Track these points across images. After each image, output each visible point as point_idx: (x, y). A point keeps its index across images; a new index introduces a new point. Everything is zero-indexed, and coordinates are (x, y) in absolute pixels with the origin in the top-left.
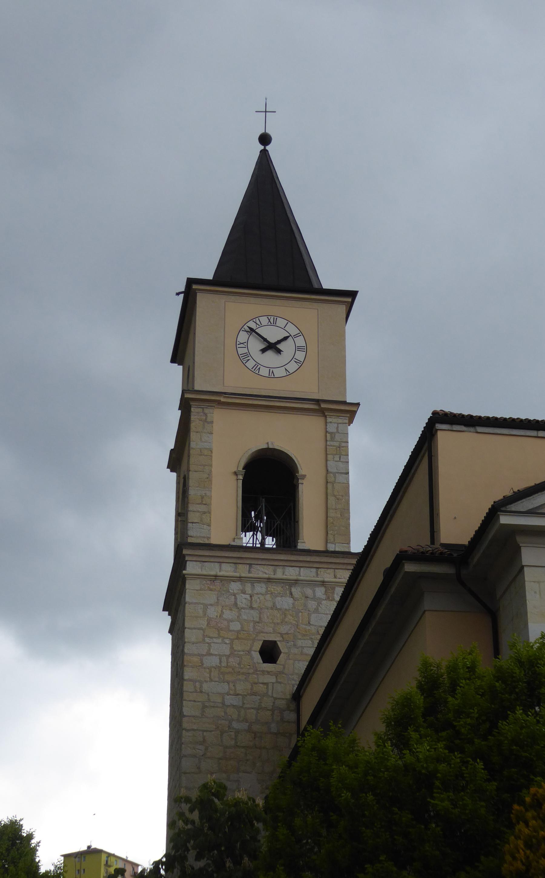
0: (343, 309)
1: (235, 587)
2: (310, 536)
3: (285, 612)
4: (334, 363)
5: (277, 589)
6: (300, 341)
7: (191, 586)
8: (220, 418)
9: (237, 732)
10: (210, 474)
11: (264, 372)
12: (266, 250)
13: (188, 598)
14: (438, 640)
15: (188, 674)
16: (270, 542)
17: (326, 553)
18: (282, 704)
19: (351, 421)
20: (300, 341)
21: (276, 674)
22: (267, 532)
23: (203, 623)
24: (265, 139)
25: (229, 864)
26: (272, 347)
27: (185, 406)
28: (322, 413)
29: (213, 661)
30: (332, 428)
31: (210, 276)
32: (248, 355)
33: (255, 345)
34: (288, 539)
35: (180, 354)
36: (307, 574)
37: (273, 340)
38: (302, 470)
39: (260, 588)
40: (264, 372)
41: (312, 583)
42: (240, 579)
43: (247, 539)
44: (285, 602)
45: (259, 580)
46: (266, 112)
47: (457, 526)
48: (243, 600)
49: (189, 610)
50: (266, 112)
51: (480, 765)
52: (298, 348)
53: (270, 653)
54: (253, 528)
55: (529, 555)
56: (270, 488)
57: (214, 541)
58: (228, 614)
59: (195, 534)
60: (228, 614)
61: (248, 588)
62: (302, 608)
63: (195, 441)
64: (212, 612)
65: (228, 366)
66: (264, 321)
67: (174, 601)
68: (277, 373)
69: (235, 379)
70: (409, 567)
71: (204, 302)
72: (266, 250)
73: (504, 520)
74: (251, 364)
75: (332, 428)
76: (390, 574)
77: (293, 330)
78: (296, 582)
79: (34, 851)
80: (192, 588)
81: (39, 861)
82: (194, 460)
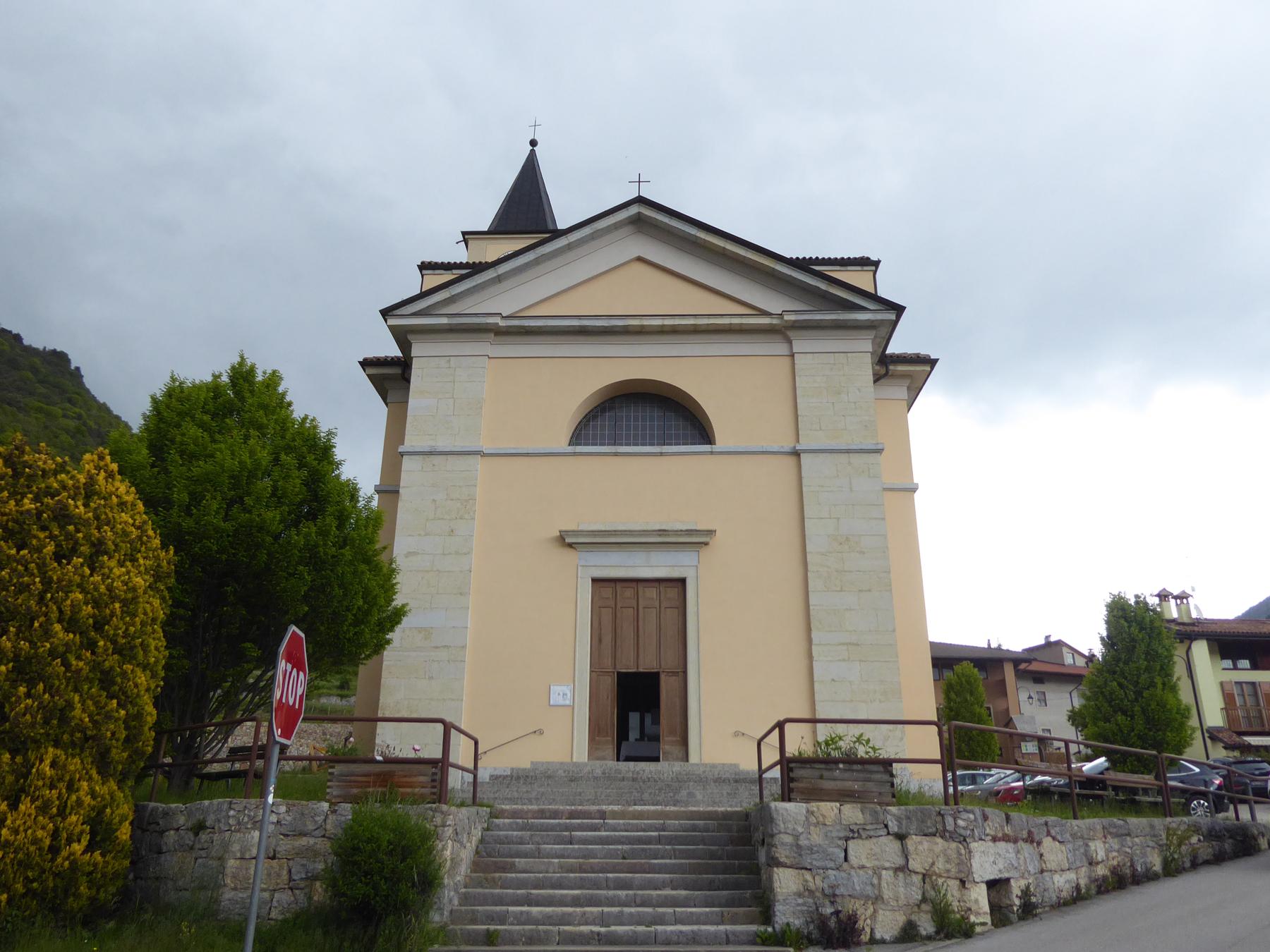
24: (533, 143)
37: (791, 461)
46: (796, 454)
79: (1211, 652)
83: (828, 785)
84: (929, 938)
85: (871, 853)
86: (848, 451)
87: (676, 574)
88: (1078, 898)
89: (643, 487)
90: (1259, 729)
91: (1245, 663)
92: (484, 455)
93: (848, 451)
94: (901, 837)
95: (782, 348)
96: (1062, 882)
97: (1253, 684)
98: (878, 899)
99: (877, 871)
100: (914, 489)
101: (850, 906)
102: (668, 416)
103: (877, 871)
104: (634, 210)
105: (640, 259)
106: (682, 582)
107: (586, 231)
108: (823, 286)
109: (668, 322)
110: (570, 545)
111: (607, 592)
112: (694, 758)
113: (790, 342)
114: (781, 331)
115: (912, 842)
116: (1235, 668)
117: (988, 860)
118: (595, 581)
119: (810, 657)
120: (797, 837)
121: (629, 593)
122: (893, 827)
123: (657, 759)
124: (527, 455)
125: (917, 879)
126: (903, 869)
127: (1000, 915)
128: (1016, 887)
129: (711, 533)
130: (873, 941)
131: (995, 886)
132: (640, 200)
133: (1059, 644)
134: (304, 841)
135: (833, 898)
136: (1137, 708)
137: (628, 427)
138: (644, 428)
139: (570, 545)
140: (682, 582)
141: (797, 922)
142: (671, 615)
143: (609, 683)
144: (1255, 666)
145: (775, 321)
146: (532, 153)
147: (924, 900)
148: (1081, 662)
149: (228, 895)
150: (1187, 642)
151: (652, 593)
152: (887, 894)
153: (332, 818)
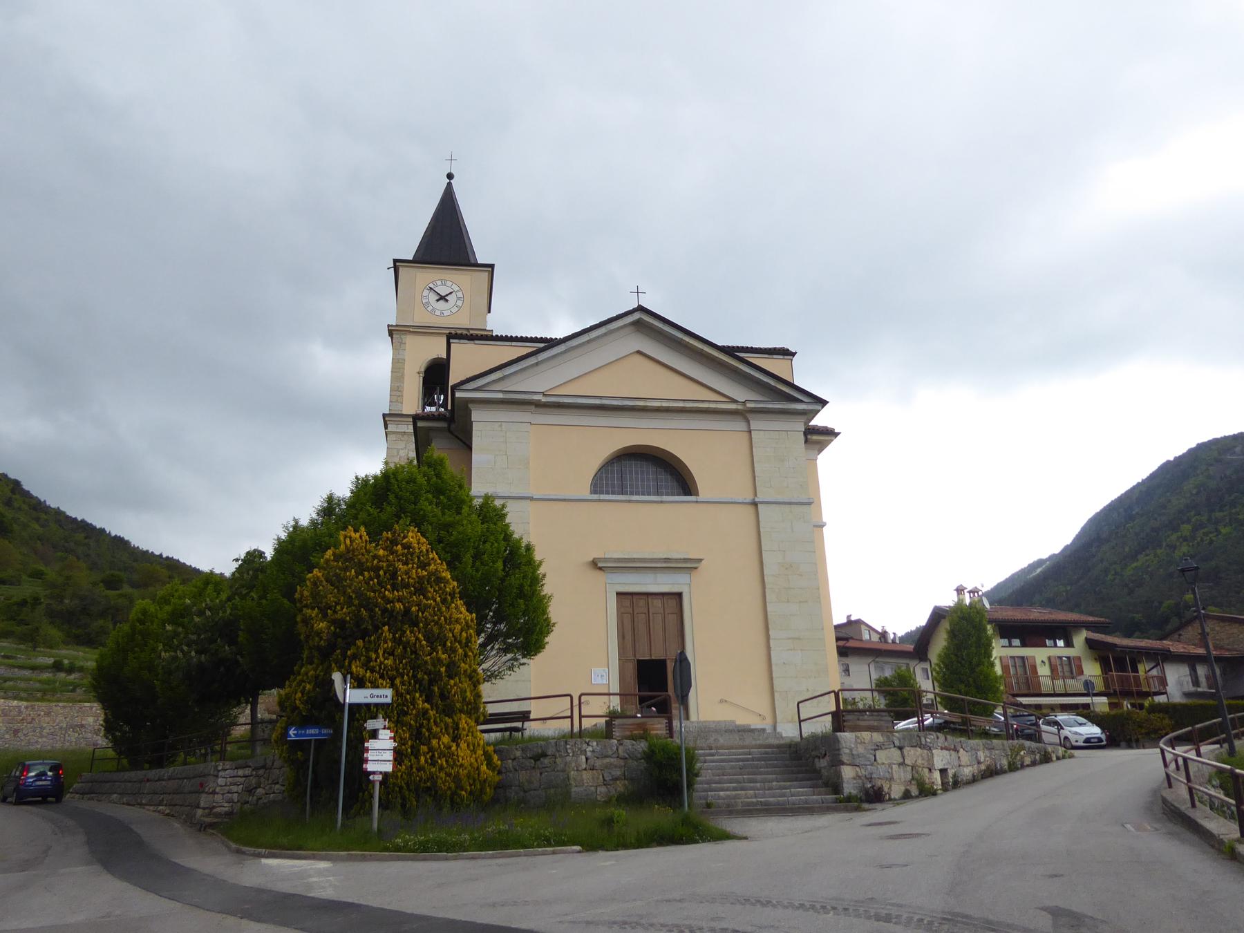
6: (460, 294)
11: (438, 313)
12: (446, 242)
20: (460, 294)
24: (450, 176)
26: (442, 298)
31: (410, 256)
32: (428, 303)
33: (433, 297)
37: (751, 509)
40: (438, 313)
46: (755, 504)
50: (755, 504)
52: (459, 299)
55: (477, 415)
57: (404, 412)
66: (439, 283)
72: (446, 242)
74: (430, 309)
77: (456, 288)
84: (917, 797)
85: (888, 756)
86: (790, 503)
87: (675, 589)
88: (974, 780)
89: (647, 526)
90: (1026, 692)
91: (1016, 642)
92: (532, 499)
93: (790, 503)
94: (901, 748)
95: (742, 426)
96: (967, 772)
97: (1022, 658)
98: (891, 779)
99: (890, 765)
100: (822, 526)
101: (879, 783)
102: (673, 476)
103: (890, 765)
104: (637, 316)
105: (639, 352)
106: (680, 595)
107: (603, 330)
108: (772, 382)
109: (665, 404)
110: (600, 569)
111: (627, 602)
112: (693, 717)
113: (748, 422)
114: (744, 414)
115: (906, 750)
116: (1010, 646)
117: (941, 759)
118: (618, 594)
119: (769, 648)
120: (851, 750)
121: (642, 602)
122: (897, 743)
124: (564, 500)
125: (909, 769)
126: (903, 764)
127: (945, 787)
128: (951, 773)
129: (701, 560)
130: (890, 799)
131: (943, 772)
132: (641, 309)
133: (859, 622)
134: (608, 760)
135: (870, 779)
136: (460, 651)
137: (631, 479)
138: (643, 480)
139: (600, 569)
140: (680, 595)
141: (854, 792)
142: (672, 619)
143: (631, 669)
144: (1024, 645)
145: (740, 407)
146: (449, 185)
147: (913, 778)
148: (875, 638)
149: (574, 789)
151: (657, 603)
152: (896, 776)
153: (621, 748)
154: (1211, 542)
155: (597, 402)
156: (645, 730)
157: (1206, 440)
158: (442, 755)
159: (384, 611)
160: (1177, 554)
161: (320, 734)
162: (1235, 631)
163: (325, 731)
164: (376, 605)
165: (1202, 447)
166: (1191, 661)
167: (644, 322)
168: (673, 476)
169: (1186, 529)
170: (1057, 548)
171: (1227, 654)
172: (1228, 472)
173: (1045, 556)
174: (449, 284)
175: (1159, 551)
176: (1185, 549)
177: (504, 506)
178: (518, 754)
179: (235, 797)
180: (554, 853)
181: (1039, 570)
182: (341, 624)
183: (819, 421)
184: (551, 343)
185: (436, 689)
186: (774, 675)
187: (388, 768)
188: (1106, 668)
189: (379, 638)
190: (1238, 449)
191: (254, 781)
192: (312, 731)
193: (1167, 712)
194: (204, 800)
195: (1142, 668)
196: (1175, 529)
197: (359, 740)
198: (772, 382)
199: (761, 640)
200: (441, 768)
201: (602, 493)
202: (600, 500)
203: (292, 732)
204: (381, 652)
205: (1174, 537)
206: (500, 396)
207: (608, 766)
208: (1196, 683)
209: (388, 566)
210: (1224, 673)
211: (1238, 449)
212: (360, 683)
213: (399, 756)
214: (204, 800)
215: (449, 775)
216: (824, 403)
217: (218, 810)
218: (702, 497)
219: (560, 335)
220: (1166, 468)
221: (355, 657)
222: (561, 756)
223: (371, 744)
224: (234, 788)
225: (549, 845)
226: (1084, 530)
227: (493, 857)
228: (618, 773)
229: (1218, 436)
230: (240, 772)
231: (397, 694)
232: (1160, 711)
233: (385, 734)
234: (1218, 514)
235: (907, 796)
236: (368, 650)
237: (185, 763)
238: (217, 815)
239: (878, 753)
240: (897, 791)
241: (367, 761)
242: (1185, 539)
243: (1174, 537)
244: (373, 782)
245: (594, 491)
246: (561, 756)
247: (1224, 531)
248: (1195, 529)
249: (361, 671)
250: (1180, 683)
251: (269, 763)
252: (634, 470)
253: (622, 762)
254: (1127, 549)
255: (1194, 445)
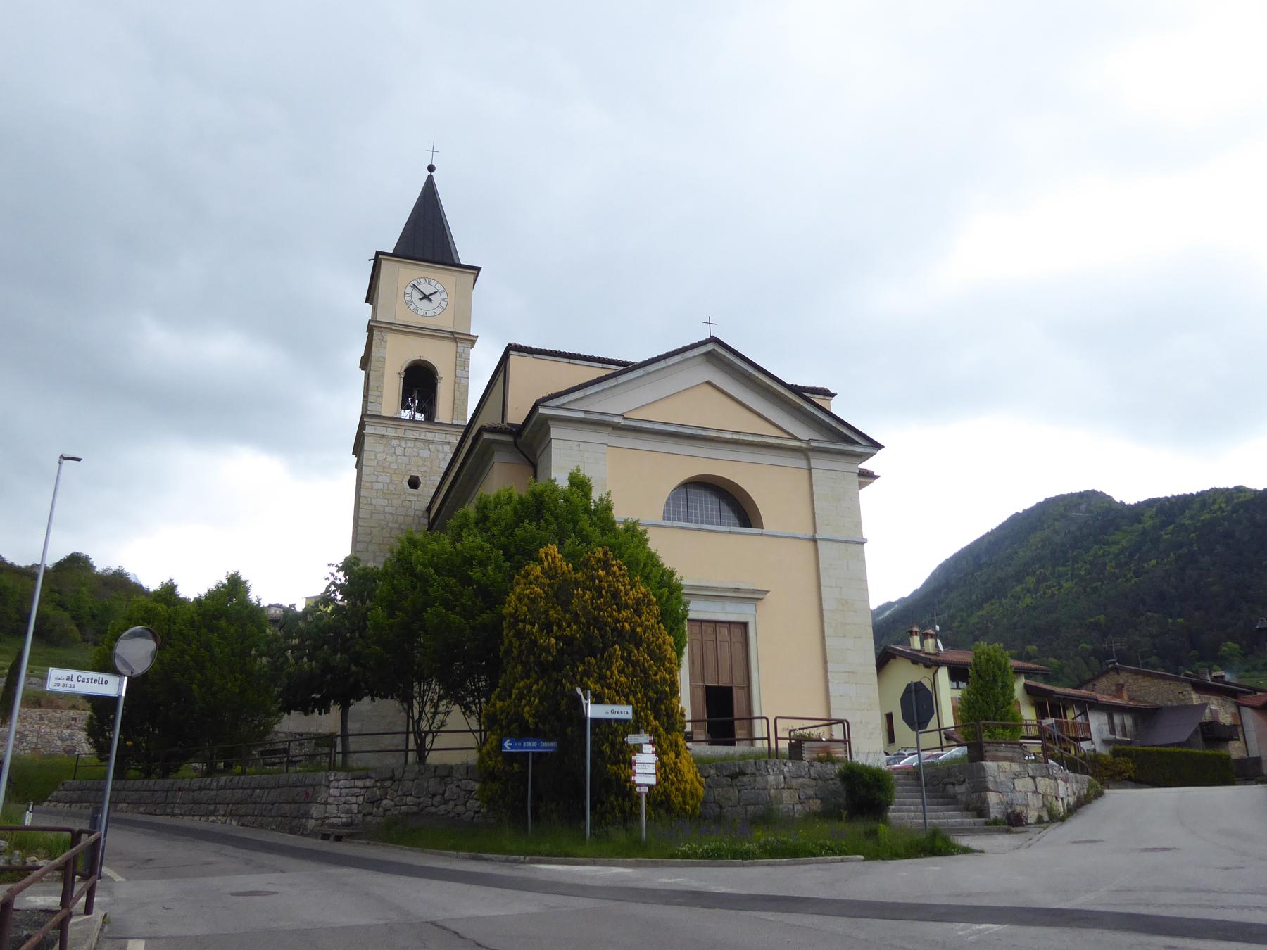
0: (472, 277)
1: (395, 442)
2: (443, 414)
3: (424, 459)
4: (464, 312)
5: (421, 445)
6: (444, 295)
7: (367, 441)
8: (391, 338)
9: (392, 529)
10: (383, 375)
11: (421, 312)
12: (426, 237)
13: (366, 447)
14: (501, 481)
15: (363, 493)
16: (419, 417)
17: (452, 425)
18: (420, 513)
19: (472, 346)
21: (418, 496)
22: (418, 410)
23: (374, 463)
24: (431, 168)
25: (359, 604)
26: (426, 297)
27: (370, 329)
28: (455, 340)
29: (380, 486)
30: (460, 350)
34: (430, 418)
35: (370, 298)
36: (439, 437)
37: (810, 545)
38: (440, 374)
39: (411, 444)
41: (442, 443)
42: (398, 438)
43: (405, 414)
44: (426, 453)
45: (410, 439)
46: (815, 540)
47: (516, 415)
48: (399, 451)
49: (366, 455)
50: (815, 540)
51: (501, 552)
52: (443, 300)
53: (414, 483)
54: (408, 407)
55: (556, 432)
56: (420, 383)
58: (389, 459)
59: (372, 409)
60: (389, 459)
61: (403, 444)
62: (433, 456)
63: (375, 353)
64: (380, 457)
65: (398, 308)
66: (423, 281)
67: (358, 449)
68: (428, 314)
69: (402, 316)
70: (486, 436)
71: (385, 266)
72: (426, 237)
73: (542, 411)
74: (412, 307)
75: (460, 350)
76: (475, 439)
77: (441, 289)
78: (432, 442)
79: (247, 590)
80: (368, 441)
81: (259, 600)
82: (374, 363)
83: (1001, 754)
85: (1024, 784)
87: (742, 619)
93: (846, 542)
94: (1034, 778)
95: (802, 463)
98: (1027, 805)
99: (1026, 793)
101: (1018, 809)
102: (742, 511)
104: (710, 347)
105: (708, 383)
106: (745, 625)
108: (834, 424)
109: (736, 437)
113: (809, 460)
114: (805, 452)
115: (1038, 779)
123: (733, 744)
132: (714, 340)
134: (801, 780)
140: (745, 625)
142: (737, 648)
143: (701, 693)
145: (804, 445)
146: (430, 178)
147: (1044, 805)
150: (934, 669)
151: (724, 631)
154: (1053, 595)
155: (673, 429)
156: (828, 753)
157: (1053, 495)
158: (672, 771)
159: (614, 630)
160: (1021, 605)
161: (539, 747)
162: (1147, 684)
163: (543, 744)
164: (606, 624)
165: (1049, 502)
166: (1109, 709)
167: (718, 354)
168: (742, 511)
169: (1030, 581)
170: (906, 593)
171: (1142, 705)
172: (1073, 528)
173: (894, 599)
174: (433, 282)
175: (1004, 601)
176: (1028, 600)
177: (645, 532)
178: (713, 772)
179: (355, 808)
180: (842, 861)
181: (888, 613)
182: (569, 641)
183: (867, 465)
184: (628, 367)
185: (663, 707)
186: (832, 706)
187: (652, 780)
188: (1042, 714)
189: (610, 657)
190: (1083, 507)
191: (378, 793)
192: (530, 744)
193: (1130, 757)
194: (316, 810)
195: (1070, 714)
196: (1020, 580)
197: (625, 756)
198: (834, 424)
199: (820, 673)
200: (672, 783)
201: (674, 520)
202: (672, 527)
203: (507, 744)
204: (614, 668)
205: (1018, 588)
206: (582, 415)
207: (803, 786)
208: (1113, 731)
209: (609, 586)
210: (1135, 723)
211: (1083, 507)
212: (598, 699)
213: (661, 766)
214: (316, 810)
215: (678, 790)
216: (879, 446)
217: (335, 821)
218: (767, 530)
219: (638, 359)
220: (1016, 520)
221: (586, 673)
222: (761, 775)
223: (637, 758)
224: (353, 799)
225: (834, 854)
226: (933, 575)
227: (788, 864)
228: (810, 792)
229: (1065, 492)
230: (359, 783)
231: (635, 712)
232: (1124, 755)
233: (648, 748)
234: (1061, 569)
235: (1040, 820)
236: (600, 668)
237: (243, 773)
238: (332, 825)
239: (1016, 781)
240: (1032, 820)
241: (635, 773)
242: (1029, 591)
243: (1018, 588)
244: (640, 793)
245: (667, 516)
246: (761, 775)
247: (1066, 585)
248: (1039, 582)
249: (598, 688)
250: (1101, 731)
251: (398, 774)
252: (707, 503)
253: (813, 783)
254: (974, 597)
255: (1042, 500)
